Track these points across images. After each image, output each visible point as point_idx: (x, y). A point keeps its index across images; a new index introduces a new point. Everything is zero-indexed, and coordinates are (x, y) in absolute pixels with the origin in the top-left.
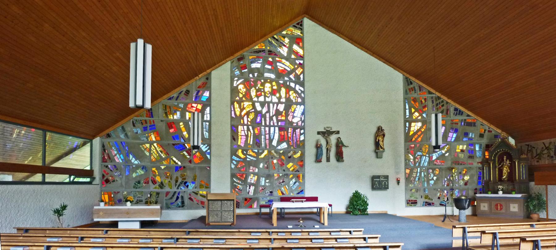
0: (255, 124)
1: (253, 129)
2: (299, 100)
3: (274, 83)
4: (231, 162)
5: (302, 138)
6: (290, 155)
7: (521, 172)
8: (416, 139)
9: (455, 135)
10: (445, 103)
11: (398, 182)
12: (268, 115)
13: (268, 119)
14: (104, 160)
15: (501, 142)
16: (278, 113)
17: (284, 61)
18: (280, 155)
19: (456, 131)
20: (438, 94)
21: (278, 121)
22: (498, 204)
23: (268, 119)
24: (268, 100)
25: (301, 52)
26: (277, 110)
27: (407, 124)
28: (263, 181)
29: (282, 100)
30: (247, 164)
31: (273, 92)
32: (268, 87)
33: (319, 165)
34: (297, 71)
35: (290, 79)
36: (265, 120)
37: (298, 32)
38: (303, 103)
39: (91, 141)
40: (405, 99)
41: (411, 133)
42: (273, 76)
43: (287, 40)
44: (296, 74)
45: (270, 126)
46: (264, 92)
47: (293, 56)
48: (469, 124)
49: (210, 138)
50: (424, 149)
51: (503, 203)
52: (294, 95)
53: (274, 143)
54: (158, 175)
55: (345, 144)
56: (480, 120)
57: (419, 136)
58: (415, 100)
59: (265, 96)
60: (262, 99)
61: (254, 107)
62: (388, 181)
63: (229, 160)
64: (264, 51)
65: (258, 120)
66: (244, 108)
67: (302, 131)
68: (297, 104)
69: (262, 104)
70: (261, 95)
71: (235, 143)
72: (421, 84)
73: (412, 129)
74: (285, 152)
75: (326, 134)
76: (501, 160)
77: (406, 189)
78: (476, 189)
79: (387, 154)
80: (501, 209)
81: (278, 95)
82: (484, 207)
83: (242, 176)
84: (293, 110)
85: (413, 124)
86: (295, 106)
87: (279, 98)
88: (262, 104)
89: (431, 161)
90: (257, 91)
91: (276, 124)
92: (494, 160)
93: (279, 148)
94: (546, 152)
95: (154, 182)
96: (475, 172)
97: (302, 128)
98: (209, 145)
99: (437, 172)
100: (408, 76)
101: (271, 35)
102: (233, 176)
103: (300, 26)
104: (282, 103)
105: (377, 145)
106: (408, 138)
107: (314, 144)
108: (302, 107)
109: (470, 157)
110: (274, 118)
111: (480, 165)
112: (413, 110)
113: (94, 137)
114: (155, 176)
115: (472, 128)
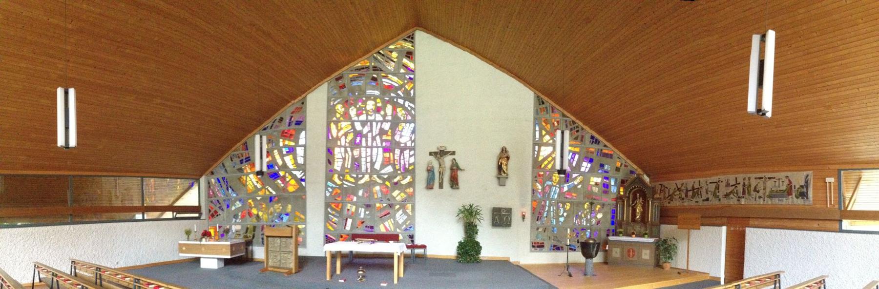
0: (354, 145)
1: (352, 151)
2: (409, 118)
3: (378, 100)
4: (326, 189)
5: (412, 160)
6: (396, 180)
7: (653, 213)
8: (546, 166)
9: (589, 165)
10: (580, 129)
11: (524, 217)
12: (370, 135)
13: (370, 140)
14: (209, 196)
15: (636, 179)
16: (382, 132)
17: (390, 76)
18: (384, 180)
19: (591, 161)
20: (573, 118)
21: (382, 141)
22: (631, 250)
23: (370, 140)
24: (370, 118)
25: (411, 65)
26: (381, 129)
27: (537, 148)
28: (362, 211)
29: (387, 118)
30: (347, 192)
31: (378, 110)
32: (370, 105)
33: (431, 191)
34: (407, 87)
35: (398, 95)
36: (367, 141)
37: (408, 45)
38: (413, 121)
39: (198, 180)
40: (535, 119)
41: (540, 158)
42: (377, 93)
43: (394, 55)
44: (406, 90)
45: (372, 147)
46: (366, 110)
47: (402, 71)
48: (606, 155)
49: (305, 164)
50: (554, 178)
51: (635, 249)
52: (403, 112)
53: (377, 166)
54: (255, 207)
55: (461, 167)
56: (618, 153)
57: (549, 162)
58: (546, 122)
59: (367, 115)
60: (363, 117)
61: (353, 127)
62: (510, 215)
63: (324, 185)
64: (368, 68)
65: (358, 140)
66: (341, 129)
67: (412, 153)
68: (406, 122)
69: (364, 123)
70: (362, 114)
71: (330, 167)
72: (554, 104)
73: (541, 154)
74: (391, 177)
75: (440, 154)
76: (635, 198)
77: (531, 227)
78: (608, 230)
79: (512, 182)
80: (633, 255)
81: (382, 113)
82: (616, 253)
83: (337, 206)
84: (400, 128)
85: (543, 148)
86: (403, 124)
87: (385, 115)
88: (364, 123)
89: (561, 194)
90: (358, 110)
91: (379, 145)
92: (629, 197)
93: (383, 172)
94: (677, 193)
95: (250, 214)
96: (608, 209)
97: (412, 149)
98: (304, 171)
99: (568, 208)
100: (540, 94)
101: (376, 50)
102: (327, 205)
103: (411, 38)
104: (387, 121)
105: (500, 168)
106: (537, 164)
107: (425, 168)
108: (413, 125)
109: (605, 192)
110: (378, 138)
111: (614, 202)
112: (544, 133)
113: (201, 176)
114: (251, 208)
115: (609, 160)
